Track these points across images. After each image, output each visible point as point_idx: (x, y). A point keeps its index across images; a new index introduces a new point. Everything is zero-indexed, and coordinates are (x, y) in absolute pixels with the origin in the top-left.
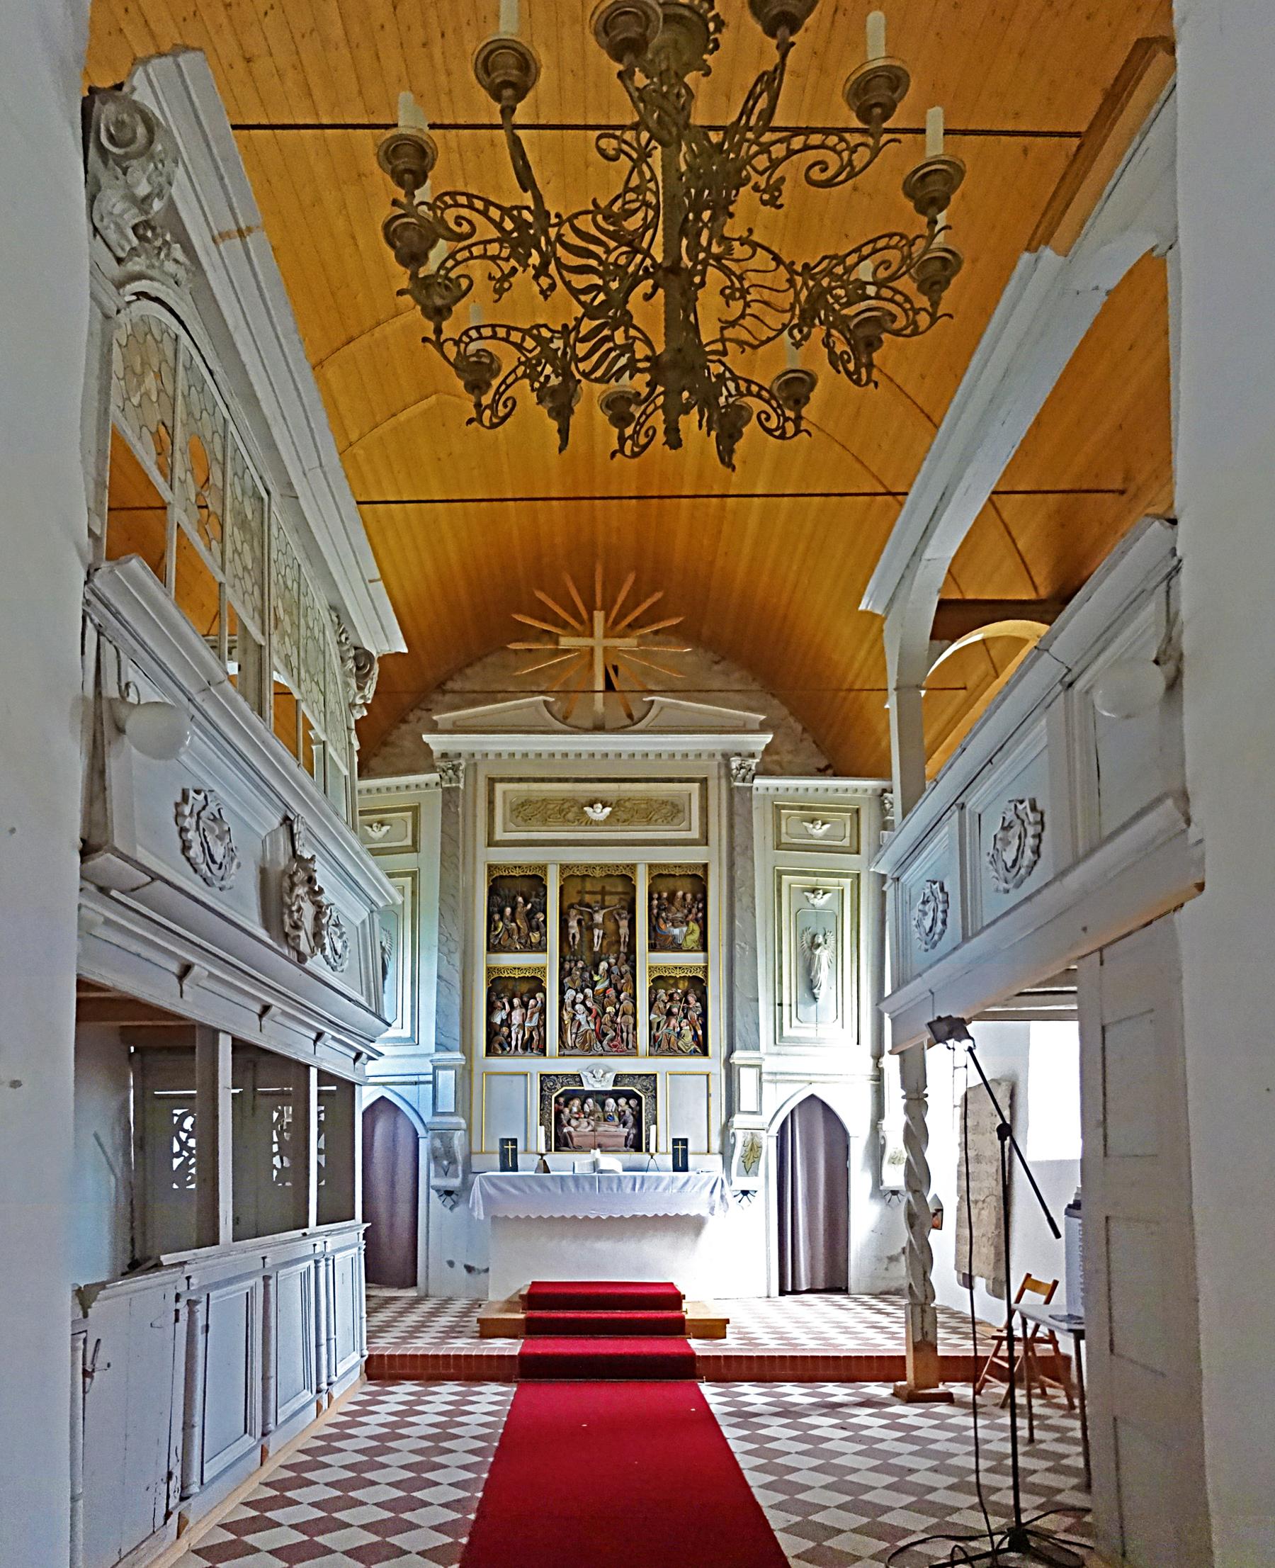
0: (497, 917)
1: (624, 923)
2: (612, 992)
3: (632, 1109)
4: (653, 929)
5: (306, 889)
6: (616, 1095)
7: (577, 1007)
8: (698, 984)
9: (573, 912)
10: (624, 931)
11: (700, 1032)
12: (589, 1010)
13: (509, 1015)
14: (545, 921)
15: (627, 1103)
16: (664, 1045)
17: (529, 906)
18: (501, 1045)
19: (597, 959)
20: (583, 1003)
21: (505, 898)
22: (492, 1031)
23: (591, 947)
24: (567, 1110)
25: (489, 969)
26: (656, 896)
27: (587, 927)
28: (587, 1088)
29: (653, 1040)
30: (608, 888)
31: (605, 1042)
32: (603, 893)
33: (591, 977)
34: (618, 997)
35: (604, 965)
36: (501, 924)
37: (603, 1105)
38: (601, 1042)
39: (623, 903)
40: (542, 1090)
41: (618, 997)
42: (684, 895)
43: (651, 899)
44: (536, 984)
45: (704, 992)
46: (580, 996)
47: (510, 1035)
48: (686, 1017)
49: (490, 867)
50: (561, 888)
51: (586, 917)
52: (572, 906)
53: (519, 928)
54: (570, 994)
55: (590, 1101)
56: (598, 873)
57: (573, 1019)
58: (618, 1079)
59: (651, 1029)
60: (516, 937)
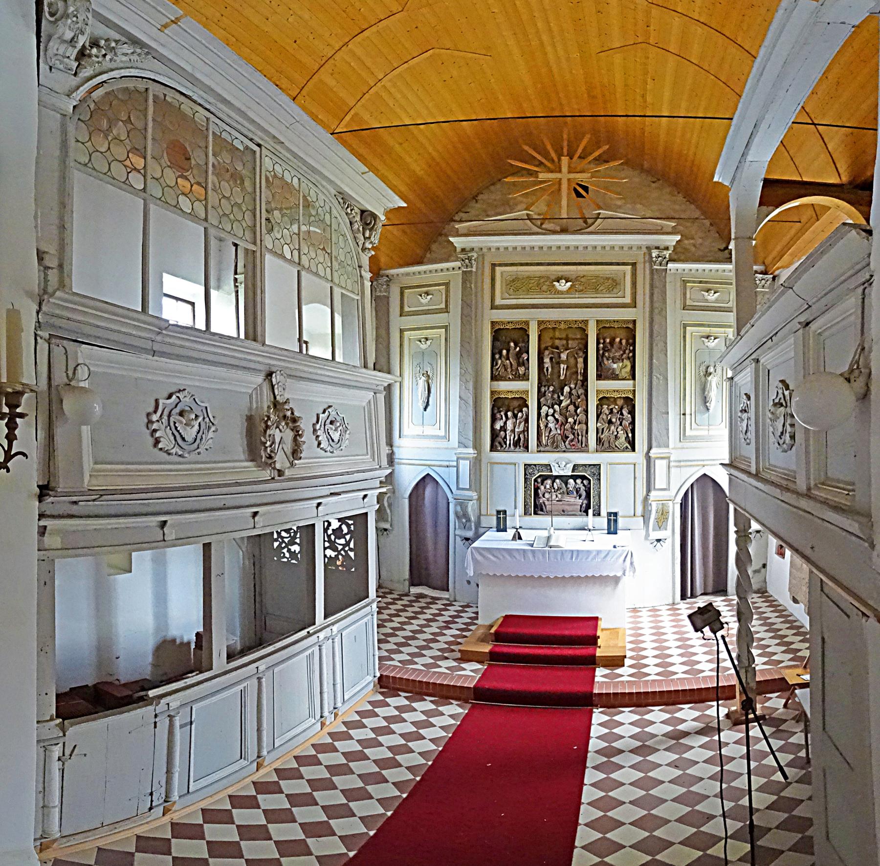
0: (497, 356)
1: (581, 360)
2: (571, 408)
3: (585, 490)
6: (575, 478)
7: (549, 418)
8: (630, 402)
9: (547, 352)
10: (580, 365)
11: (630, 435)
12: (557, 420)
13: (505, 423)
14: (528, 359)
15: (582, 482)
16: (606, 445)
17: (518, 349)
18: (500, 443)
20: (553, 415)
22: (494, 434)
23: (559, 376)
24: (542, 488)
26: (602, 341)
27: (556, 362)
28: (555, 473)
29: (599, 441)
31: (567, 442)
33: (559, 397)
34: (576, 411)
35: (567, 389)
36: (500, 362)
37: (566, 484)
39: (581, 346)
40: (525, 474)
41: (576, 411)
42: (621, 340)
43: (598, 343)
46: (551, 411)
47: (505, 437)
48: (621, 424)
50: (539, 336)
51: (556, 356)
54: (544, 409)
55: (557, 481)
60: (509, 370)
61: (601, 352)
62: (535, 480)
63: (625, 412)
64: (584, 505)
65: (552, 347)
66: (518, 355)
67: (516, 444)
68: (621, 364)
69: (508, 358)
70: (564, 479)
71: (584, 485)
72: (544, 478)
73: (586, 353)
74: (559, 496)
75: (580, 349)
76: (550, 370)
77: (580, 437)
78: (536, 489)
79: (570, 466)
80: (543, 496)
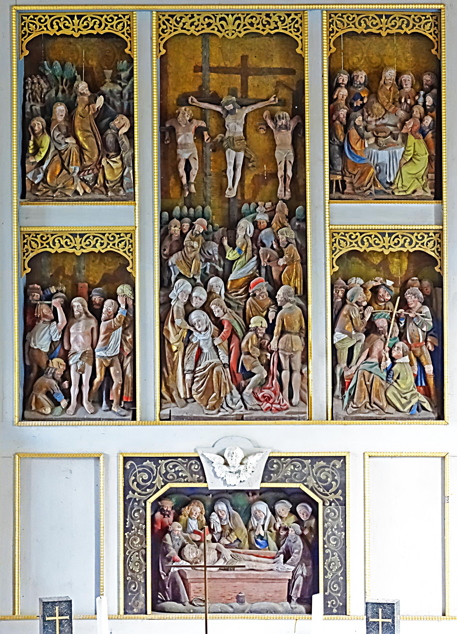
0: (38, 124)
1: (284, 137)
2: (261, 287)
4: (339, 150)
5: (362, 82)
6: (272, 497)
7: (193, 316)
9: (185, 113)
10: (284, 154)
11: (429, 369)
12: (219, 323)
13: (65, 331)
14: (130, 134)
15: (293, 511)
16: (361, 398)
17: (100, 101)
18: (49, 394)
19: (232, 218)
20: (205, 308)
21: (54, 82)
23: (222, 188)
24: (177, 527)
25: (23, 236)
26: (344, 78)
27: (214, 146)
28: (214, 484)
29: (340, 384)
30: (253, 61)
31: (248, 391)
32: (244, 70)
33: (222, 252)
34: (272, 296)
35: (245, 227)
36: (46, 141)
37: (247, 514)
38: (241, 390)
39: (284, 93)
40: (127, 488)
41: (272, 296)
42: (399, 74)
43: (333, 87)
44: (119, 272)
45: (438, 283)
46: (200, 295)
47: (66, 376)
48: (402, 336)
49: (22, 15)
50: (163, 61)
51: (213, 122)
52: (183, 101)
53: (81, 149)
54: (181, 288)
55: (221, 506)
56: (231, 30)
57: (187, 342)
58: (273, 465)
59: (335, 362)
60: (75, 168)
61: (343, 113)
62: (156, 507)
63: (414, 297)
64: (299, 581)
65: (200, 97)
66: (102, 120)
67: (100, 395)
68: (400, 151)
69: (70, 132)
70: (242, 500)
71: (299, 521)
72: (185, 499)
73: (298, 112)
74: (227, 553)
75: (282, 103)
76: (195, 165)
77: (285, 374)
78: (160, 533)
79: (257, 463)
80: (180, 553)
